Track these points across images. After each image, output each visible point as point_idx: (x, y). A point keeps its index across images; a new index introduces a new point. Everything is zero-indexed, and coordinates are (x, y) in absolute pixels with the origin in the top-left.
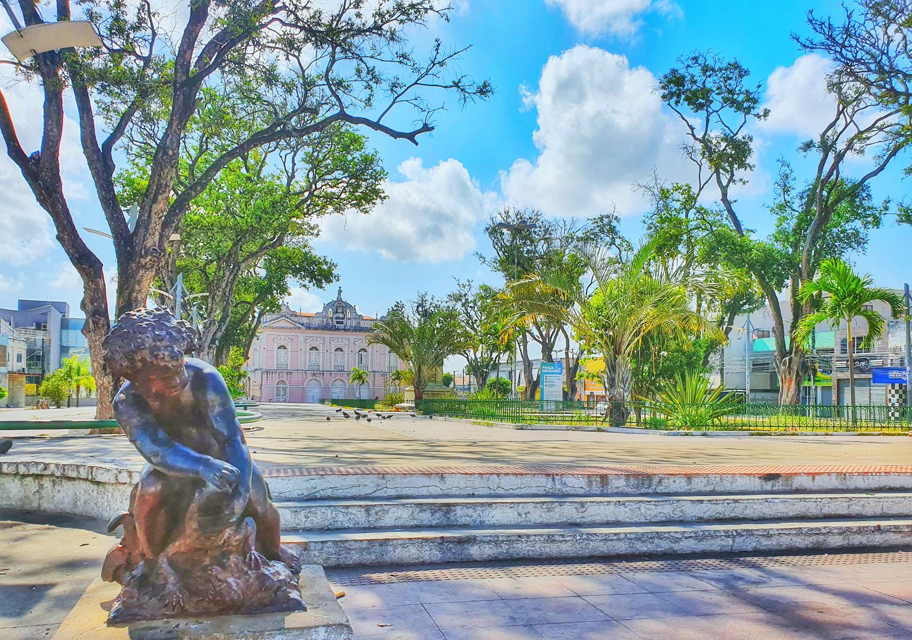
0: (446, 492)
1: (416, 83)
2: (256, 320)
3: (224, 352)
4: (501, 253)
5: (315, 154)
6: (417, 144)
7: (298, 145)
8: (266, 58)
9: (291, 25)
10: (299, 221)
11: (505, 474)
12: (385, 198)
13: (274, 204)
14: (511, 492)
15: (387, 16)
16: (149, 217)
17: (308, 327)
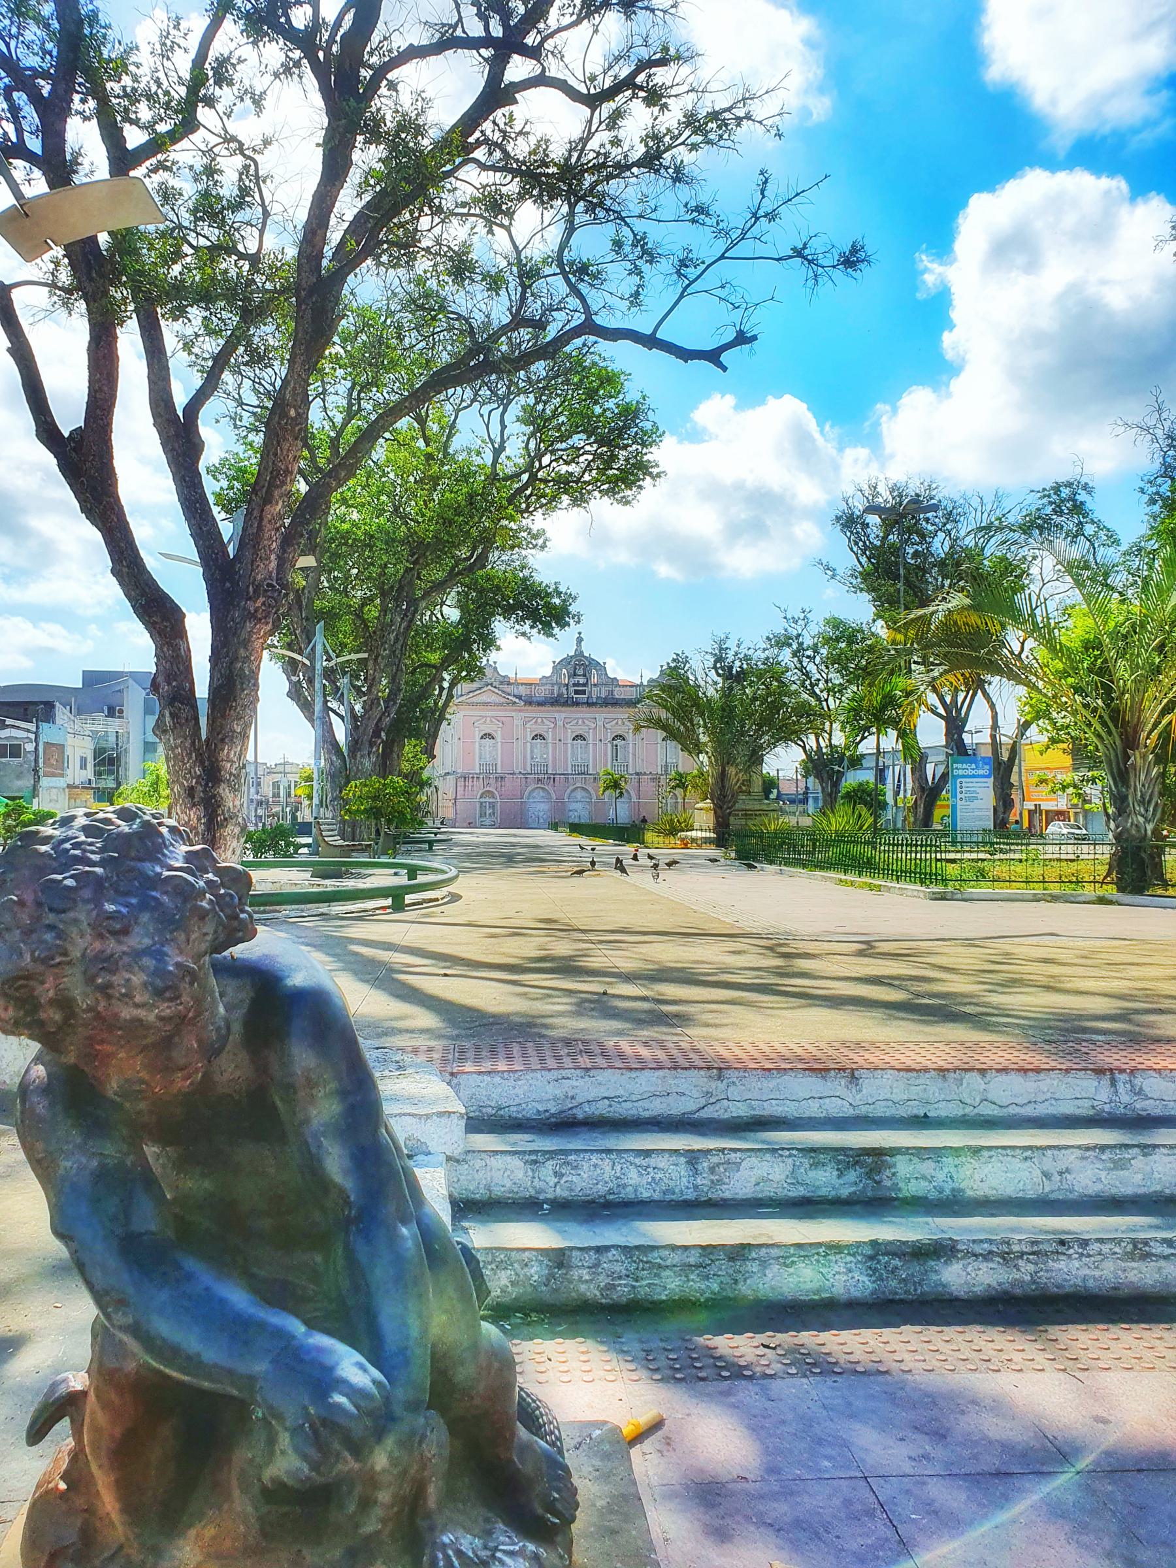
0: (863, 1110)
1: (722, 257)
2: (445, 693)
3: (396, 749)
4: (864, 560)
5: (540, 407)
6: (724, 369)
7: (510, 393)
8: (456, 233)
9: (494, 168)
10: (513, 525)
11: (998, 1071)
12: (658, 475)
13: (471, 497)
14: (1013, 1110)
15: (667, 139)
16: (260, 528)
17: (529, 702)
